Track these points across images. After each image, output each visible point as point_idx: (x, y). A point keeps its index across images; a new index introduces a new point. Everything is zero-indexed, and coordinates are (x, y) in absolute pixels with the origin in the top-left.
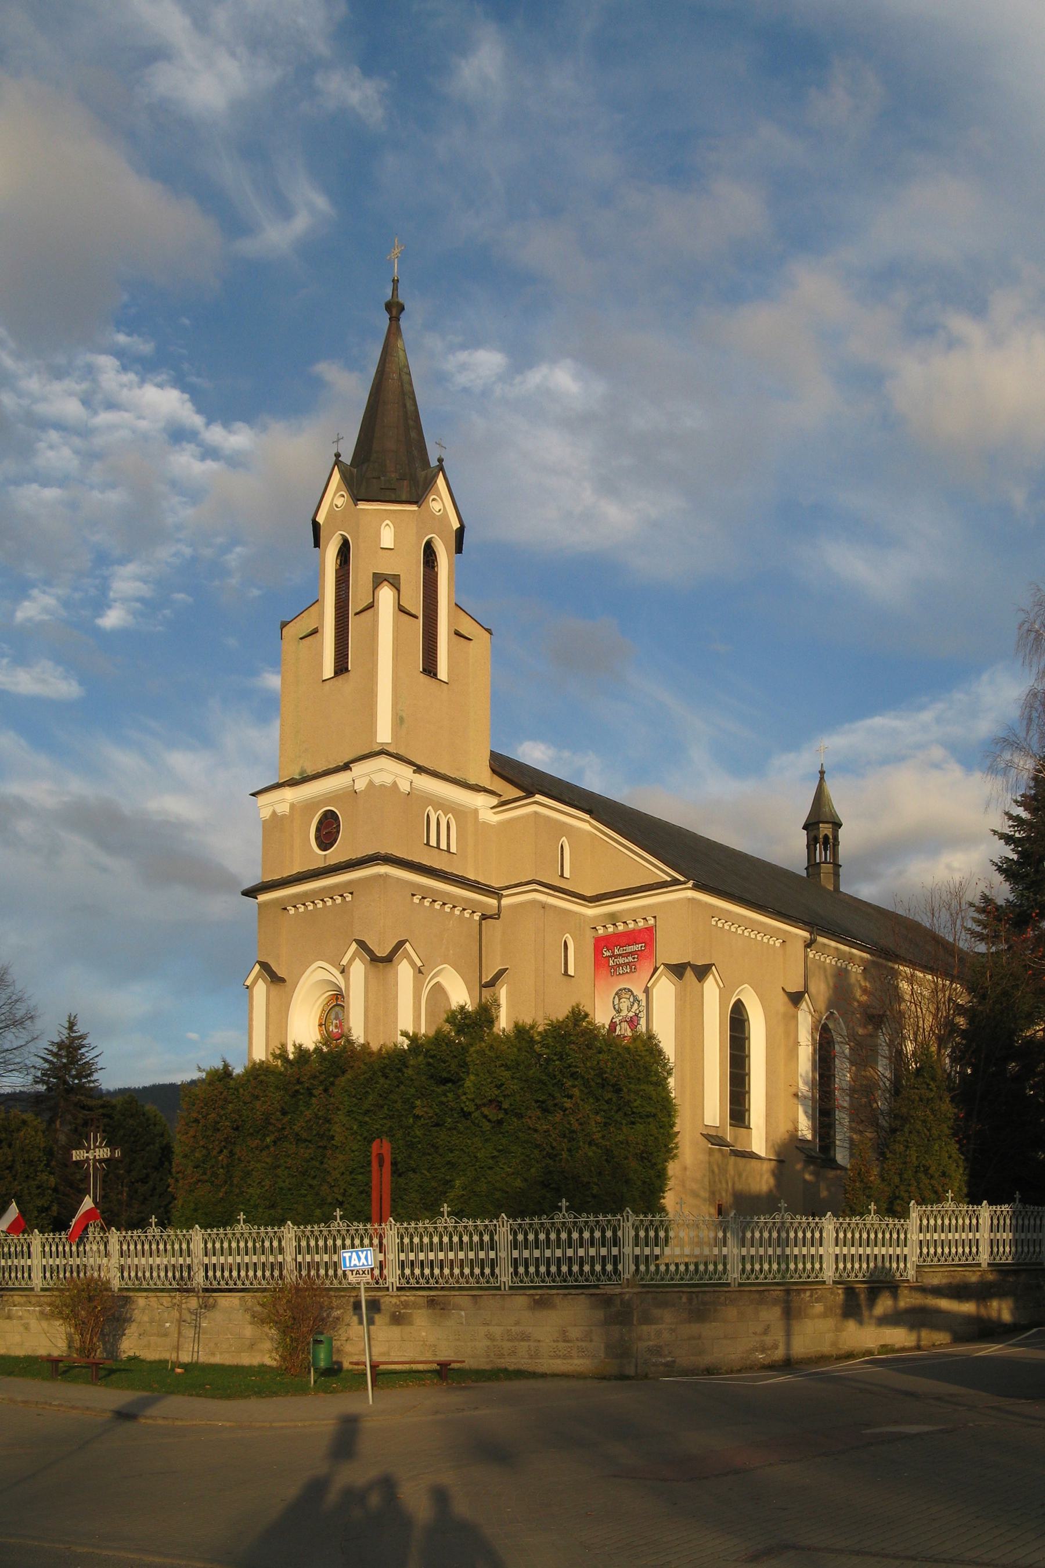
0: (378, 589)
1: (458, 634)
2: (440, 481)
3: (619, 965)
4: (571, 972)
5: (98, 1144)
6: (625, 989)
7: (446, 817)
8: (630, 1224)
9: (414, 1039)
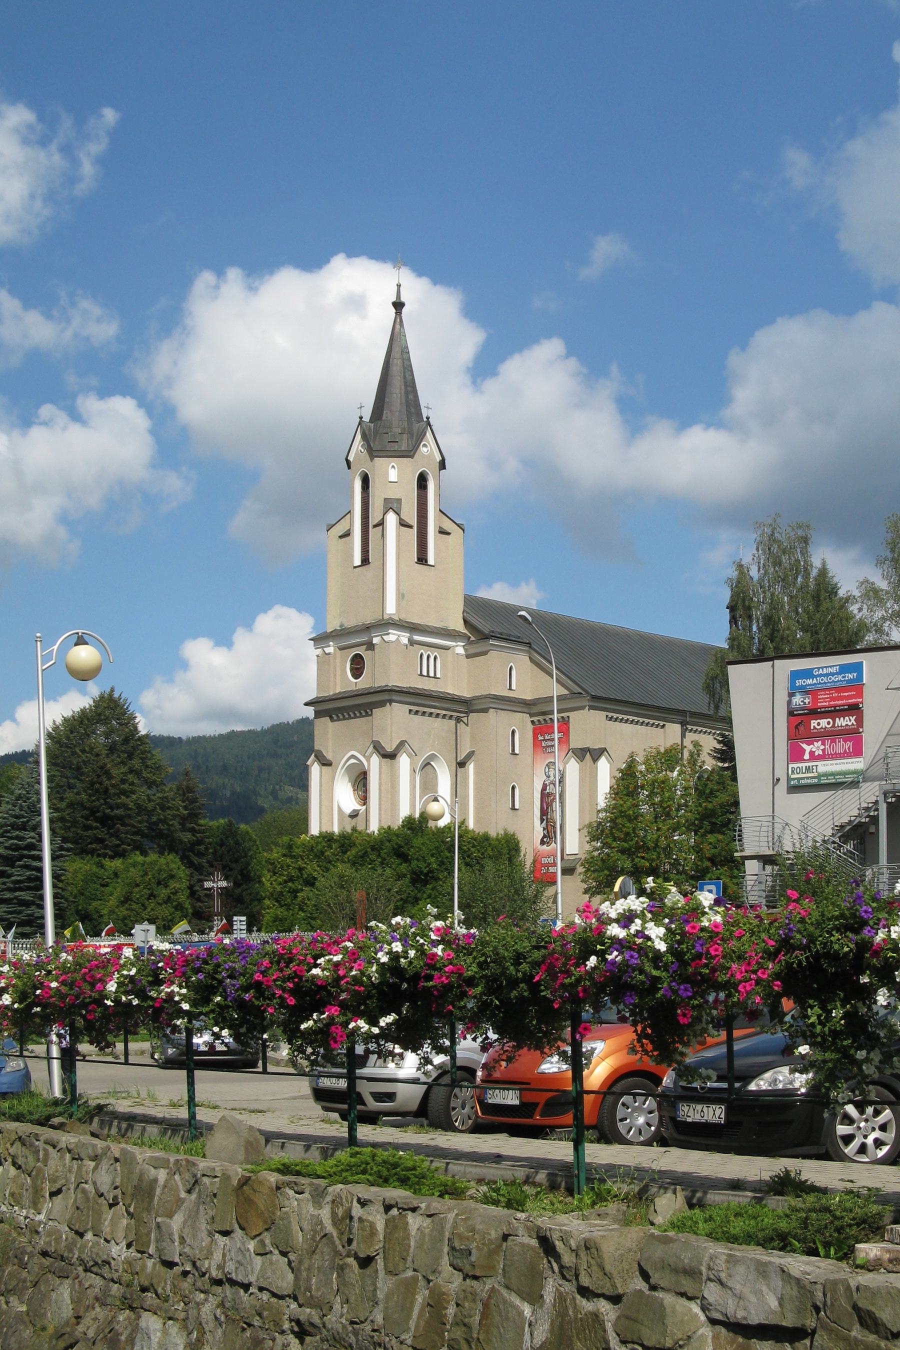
2: (429, 434)
4: (517, 751)
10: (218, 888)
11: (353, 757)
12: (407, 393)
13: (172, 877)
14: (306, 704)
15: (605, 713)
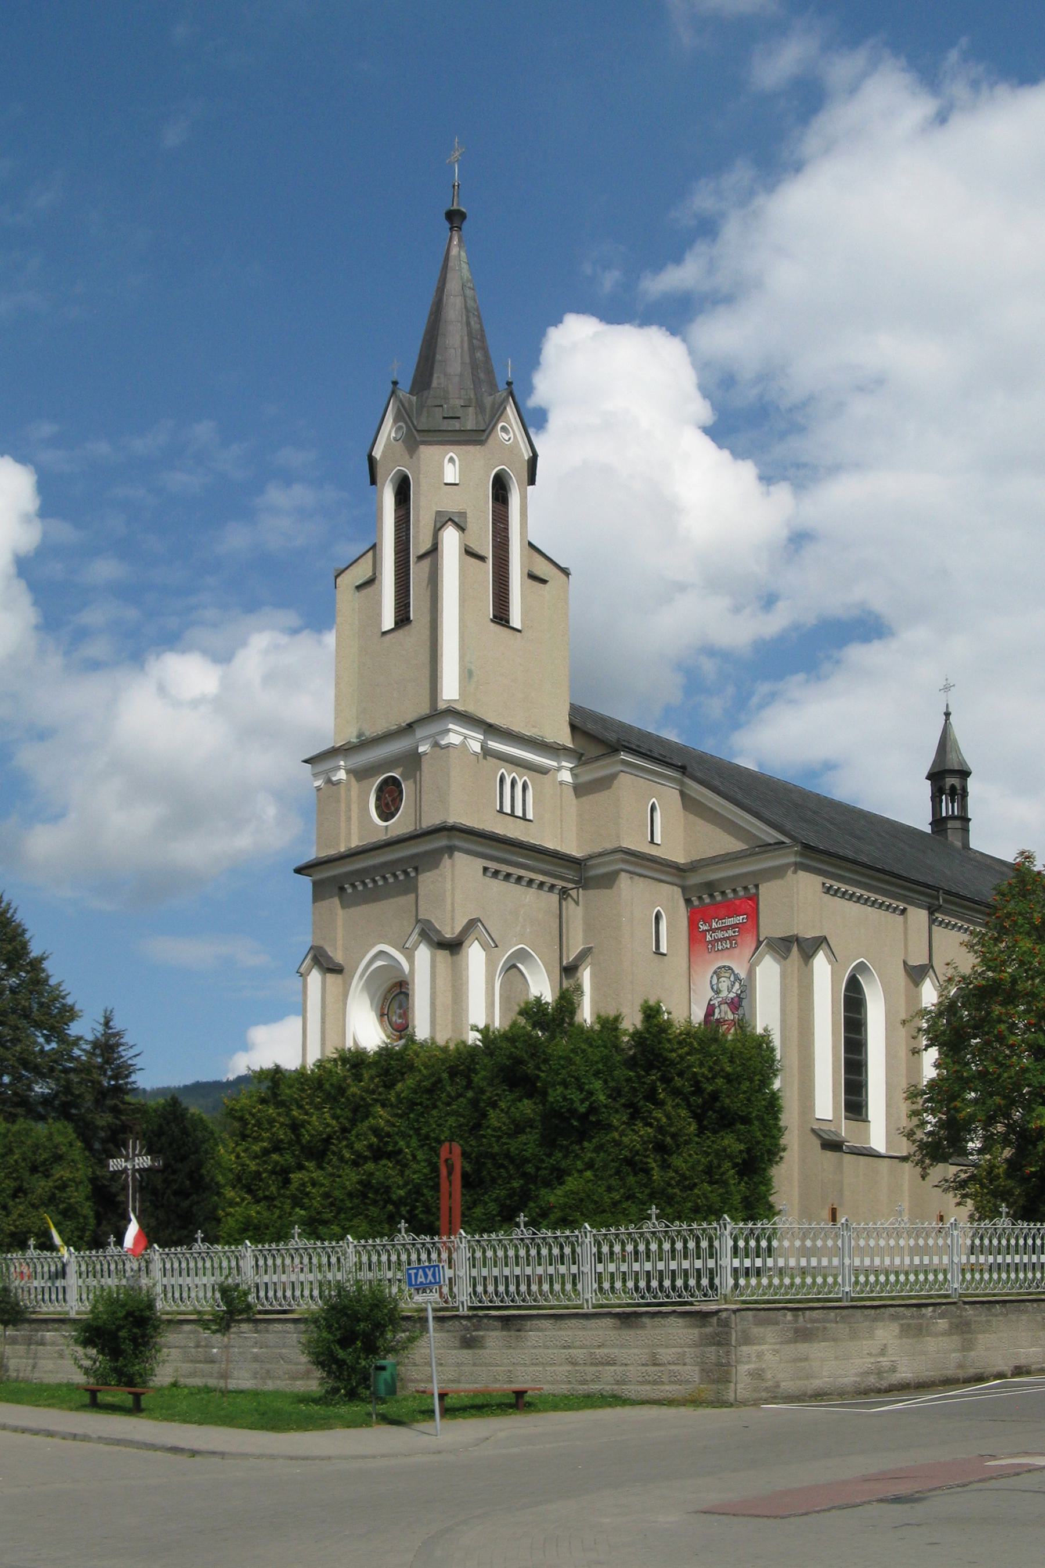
0: (440, 532)
1: (532, 577)
3: (717, 940)
4: (664, 949)
5: (137, 1152)
6: (724, 967)
7: (520, 780)
8: (727, 1232)
9: (485, 1032)
10: (134, 1170)
11: (382, 952)
12: (472, 349)
13: (58, 1158)
14: (299, 871)
15: (821, 879)
